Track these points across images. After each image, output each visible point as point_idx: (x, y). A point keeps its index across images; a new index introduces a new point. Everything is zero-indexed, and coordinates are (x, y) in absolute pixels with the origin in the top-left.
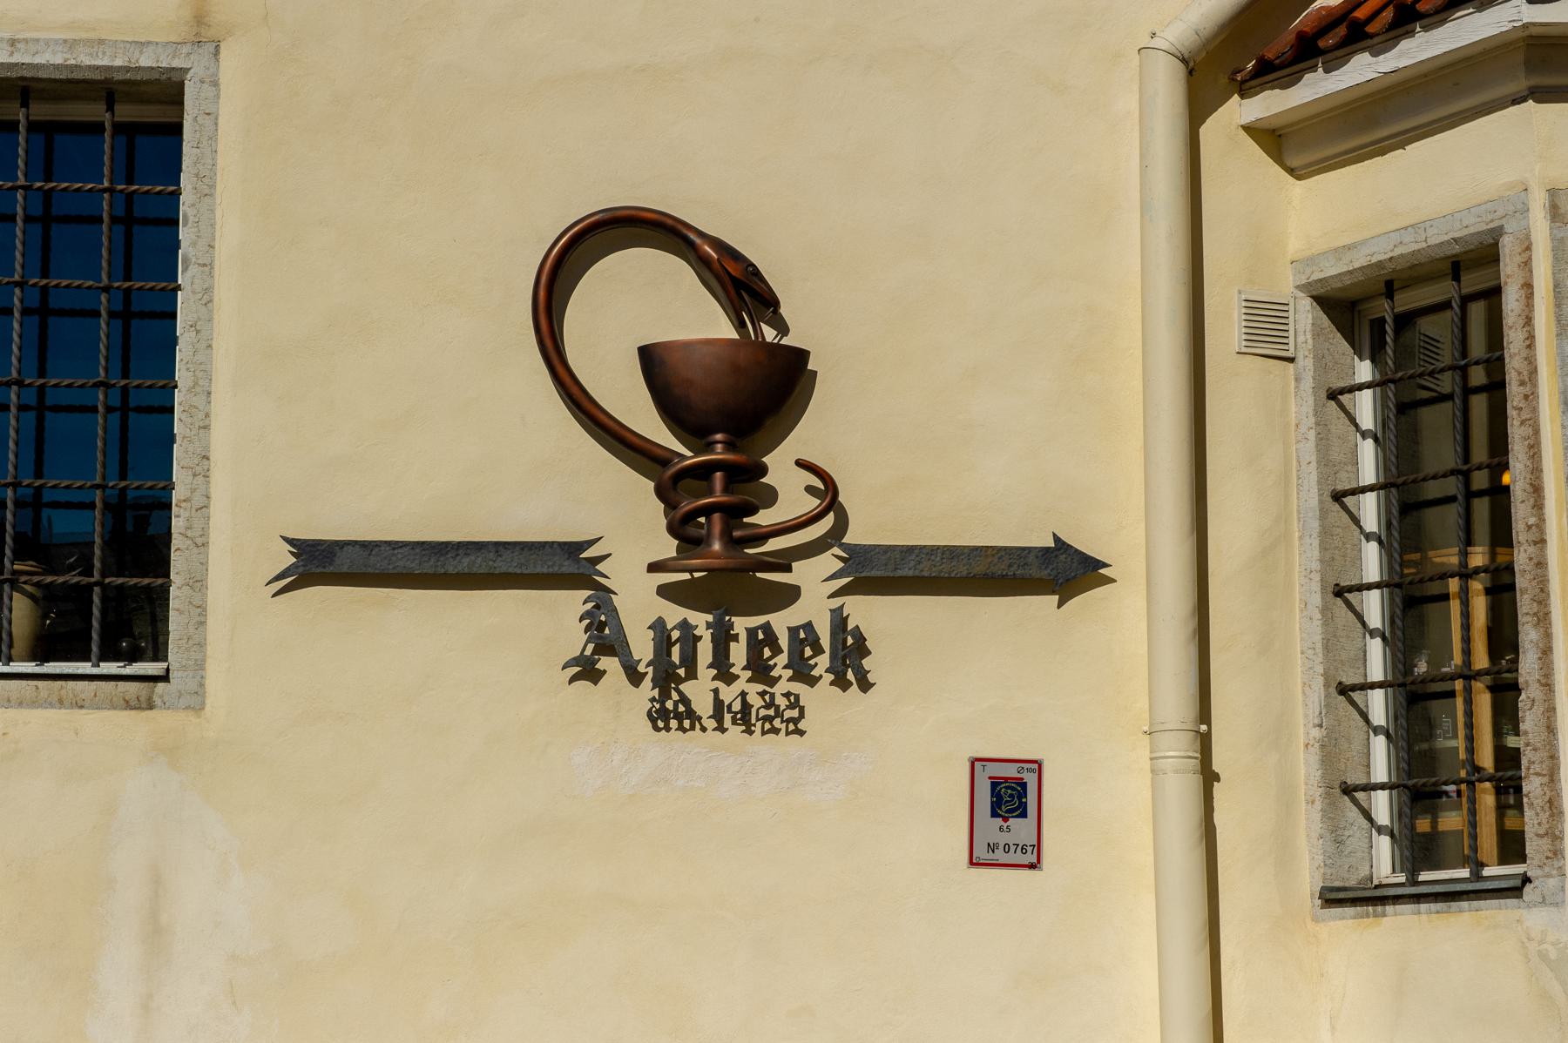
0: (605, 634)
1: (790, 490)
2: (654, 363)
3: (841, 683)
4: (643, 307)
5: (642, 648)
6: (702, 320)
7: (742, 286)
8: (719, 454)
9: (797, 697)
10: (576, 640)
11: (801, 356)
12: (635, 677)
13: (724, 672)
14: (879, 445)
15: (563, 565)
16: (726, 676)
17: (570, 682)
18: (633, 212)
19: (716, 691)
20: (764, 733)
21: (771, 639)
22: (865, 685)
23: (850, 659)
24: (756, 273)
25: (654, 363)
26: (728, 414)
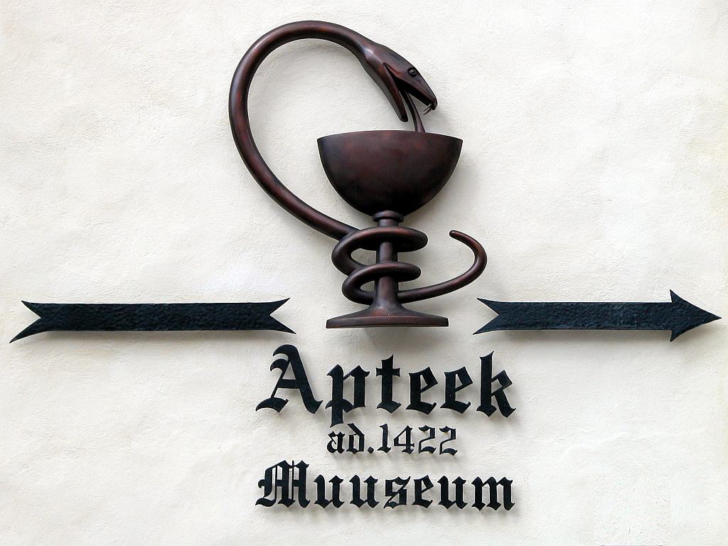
0: (291, 364)
1: (441, 259)
2: (329, 150)
3: (486, 408)
4: (323, 107)
5: (323, 390)
6: (365, 112)
7: (404, 87)
8: (385, 227)
9: (453, 432)
10: (265, 381)
11: (452, 147)
12: (312, 404)
13: (388, 404)
14: (523, 218)
15: (251, 319)
16: (388, 404)
17: (259, 407)
18: (313, 26)
19: (385, 427)
20: (420, 451)
21: (431, 380)
22: (507, 410)
23: (496, 399)
24: (413, 72)
25: (329, 150)
26: (394, 185)
